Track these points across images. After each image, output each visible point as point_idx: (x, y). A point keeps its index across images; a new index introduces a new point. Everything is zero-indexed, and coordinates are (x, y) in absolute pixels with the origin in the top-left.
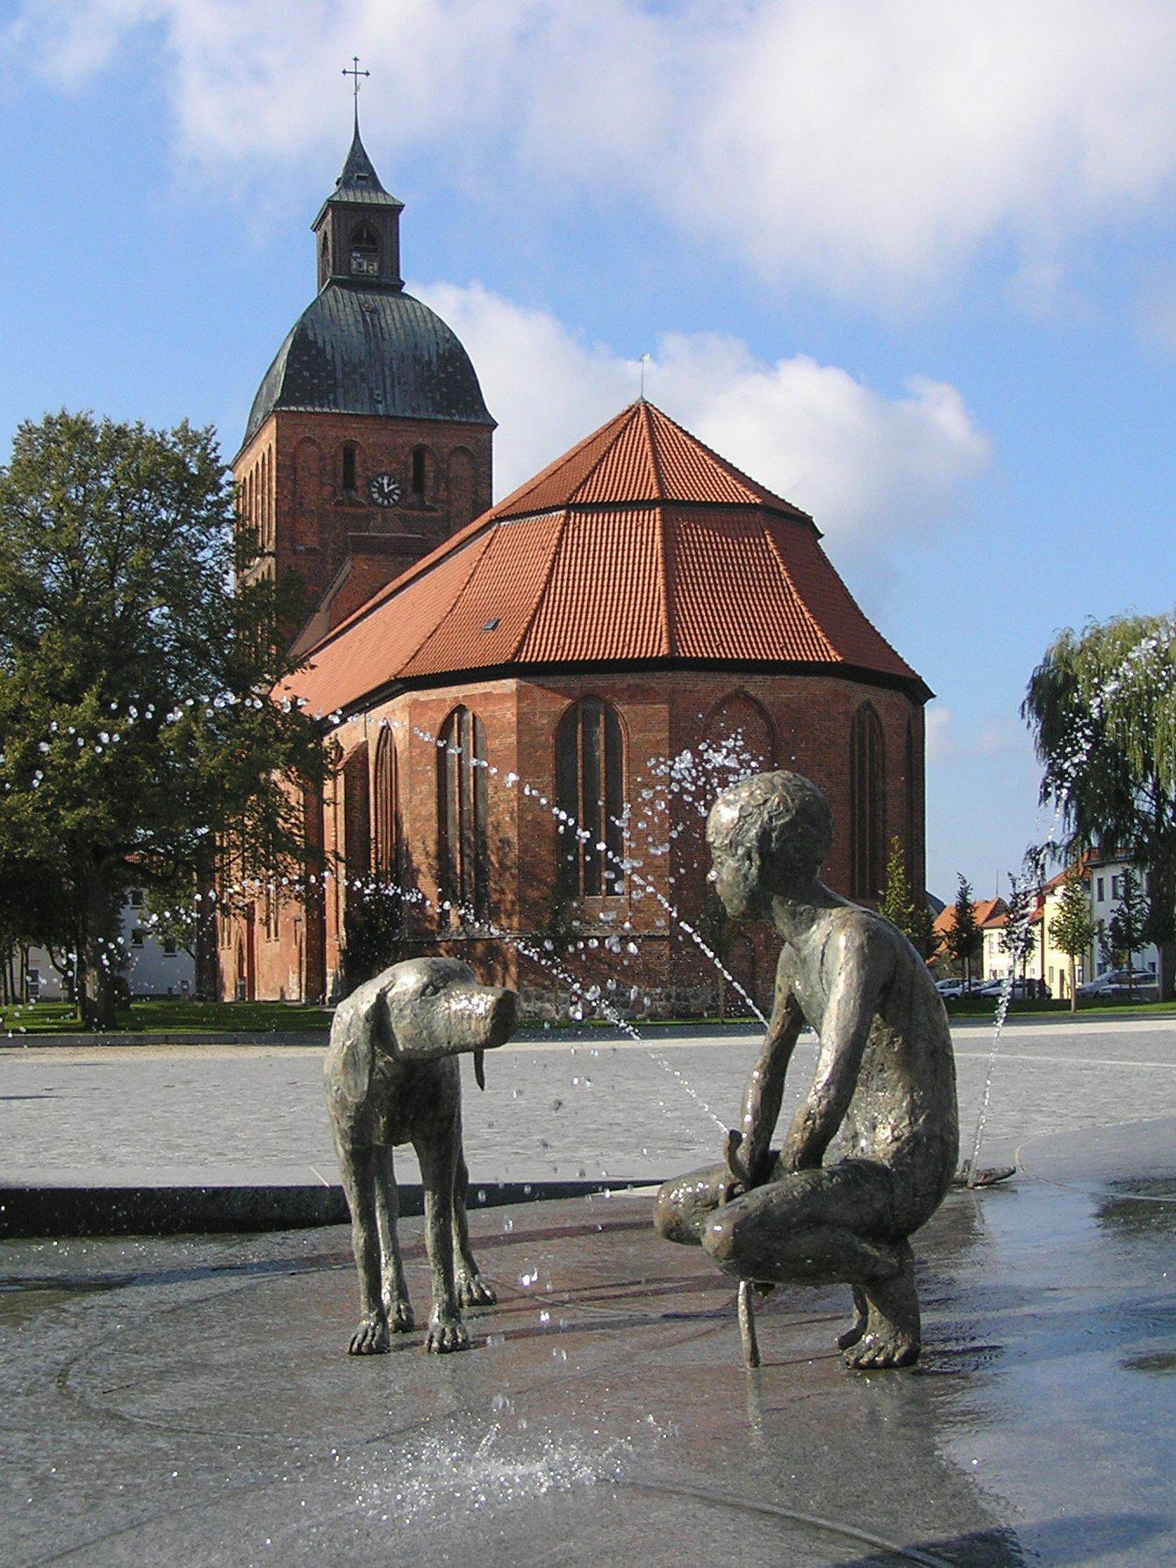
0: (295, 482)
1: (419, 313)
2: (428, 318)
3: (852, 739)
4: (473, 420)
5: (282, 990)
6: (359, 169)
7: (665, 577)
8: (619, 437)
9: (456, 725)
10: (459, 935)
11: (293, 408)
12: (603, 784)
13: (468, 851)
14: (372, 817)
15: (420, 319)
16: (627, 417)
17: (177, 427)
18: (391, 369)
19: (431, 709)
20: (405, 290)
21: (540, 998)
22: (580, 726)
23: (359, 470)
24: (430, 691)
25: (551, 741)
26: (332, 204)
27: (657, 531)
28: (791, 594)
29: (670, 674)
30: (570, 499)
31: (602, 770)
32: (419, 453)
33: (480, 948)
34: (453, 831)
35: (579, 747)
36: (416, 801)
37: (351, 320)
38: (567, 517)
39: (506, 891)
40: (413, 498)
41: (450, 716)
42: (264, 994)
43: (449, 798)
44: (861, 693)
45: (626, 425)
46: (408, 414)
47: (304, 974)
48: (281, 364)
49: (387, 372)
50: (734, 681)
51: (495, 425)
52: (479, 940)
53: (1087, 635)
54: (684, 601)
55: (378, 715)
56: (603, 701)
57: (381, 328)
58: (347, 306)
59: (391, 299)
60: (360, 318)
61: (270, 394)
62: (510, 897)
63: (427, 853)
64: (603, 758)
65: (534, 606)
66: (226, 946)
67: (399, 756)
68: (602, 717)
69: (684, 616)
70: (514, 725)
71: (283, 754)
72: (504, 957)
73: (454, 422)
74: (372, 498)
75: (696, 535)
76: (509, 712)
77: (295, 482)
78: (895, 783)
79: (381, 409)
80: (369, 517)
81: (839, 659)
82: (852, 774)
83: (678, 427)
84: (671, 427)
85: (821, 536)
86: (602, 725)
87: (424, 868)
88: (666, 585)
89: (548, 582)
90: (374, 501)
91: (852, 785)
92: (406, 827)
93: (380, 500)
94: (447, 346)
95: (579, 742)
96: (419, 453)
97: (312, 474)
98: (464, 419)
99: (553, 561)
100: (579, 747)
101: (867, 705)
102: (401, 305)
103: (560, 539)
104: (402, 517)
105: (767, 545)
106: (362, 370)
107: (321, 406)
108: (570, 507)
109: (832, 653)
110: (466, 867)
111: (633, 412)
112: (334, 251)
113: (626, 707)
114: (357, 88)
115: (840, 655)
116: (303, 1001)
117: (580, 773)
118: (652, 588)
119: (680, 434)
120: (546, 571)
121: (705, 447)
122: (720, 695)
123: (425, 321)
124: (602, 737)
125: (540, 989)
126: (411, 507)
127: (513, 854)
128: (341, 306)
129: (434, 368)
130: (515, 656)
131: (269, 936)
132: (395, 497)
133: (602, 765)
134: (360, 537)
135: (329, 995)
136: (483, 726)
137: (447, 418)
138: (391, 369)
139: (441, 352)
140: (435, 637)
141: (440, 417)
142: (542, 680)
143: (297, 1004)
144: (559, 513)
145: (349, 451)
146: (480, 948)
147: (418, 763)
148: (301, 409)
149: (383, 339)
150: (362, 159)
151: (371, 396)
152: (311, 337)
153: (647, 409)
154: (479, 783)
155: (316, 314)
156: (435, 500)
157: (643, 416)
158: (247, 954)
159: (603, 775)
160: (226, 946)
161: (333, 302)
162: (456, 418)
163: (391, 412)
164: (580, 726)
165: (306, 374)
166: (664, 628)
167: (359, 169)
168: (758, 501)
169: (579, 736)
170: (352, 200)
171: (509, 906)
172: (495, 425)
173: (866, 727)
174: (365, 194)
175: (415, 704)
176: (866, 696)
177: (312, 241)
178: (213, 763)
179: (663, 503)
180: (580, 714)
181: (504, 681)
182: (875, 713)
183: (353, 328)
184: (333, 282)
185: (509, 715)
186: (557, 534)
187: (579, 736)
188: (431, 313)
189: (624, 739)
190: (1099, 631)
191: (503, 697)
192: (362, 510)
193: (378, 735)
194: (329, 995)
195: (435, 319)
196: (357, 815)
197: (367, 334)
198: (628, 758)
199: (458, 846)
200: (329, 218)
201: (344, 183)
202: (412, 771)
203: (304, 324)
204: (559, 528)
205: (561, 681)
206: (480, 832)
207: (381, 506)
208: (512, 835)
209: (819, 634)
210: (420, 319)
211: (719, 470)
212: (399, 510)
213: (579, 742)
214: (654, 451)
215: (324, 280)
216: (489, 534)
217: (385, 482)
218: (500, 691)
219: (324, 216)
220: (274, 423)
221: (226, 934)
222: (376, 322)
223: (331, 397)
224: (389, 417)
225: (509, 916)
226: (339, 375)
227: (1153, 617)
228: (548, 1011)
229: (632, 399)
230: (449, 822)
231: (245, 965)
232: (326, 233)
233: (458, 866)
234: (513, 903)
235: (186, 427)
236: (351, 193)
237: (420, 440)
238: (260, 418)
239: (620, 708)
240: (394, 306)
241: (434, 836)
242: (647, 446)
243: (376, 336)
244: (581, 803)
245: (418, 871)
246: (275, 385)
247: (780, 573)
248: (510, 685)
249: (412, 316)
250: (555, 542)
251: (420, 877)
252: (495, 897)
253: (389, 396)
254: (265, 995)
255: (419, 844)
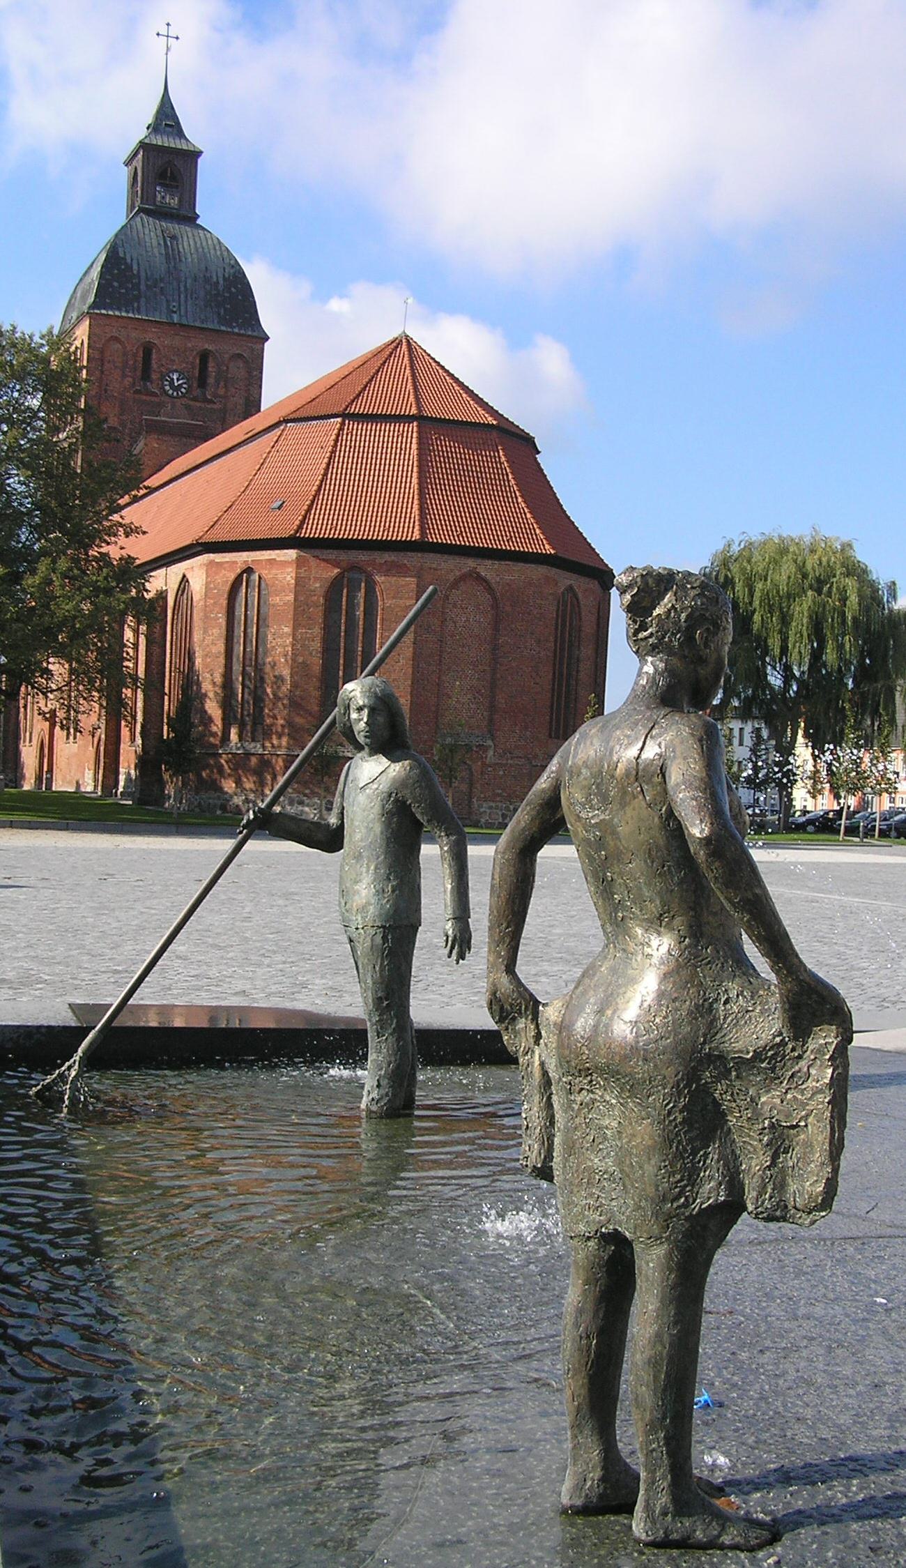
0: (102, 372)
1: (210, 242)
2: (217, 248)
3: (557, 615)
4: (250, 333)
5: (77, 783)
6: (166, 118)
7: (419, 478)
8: (385, 362)
9: (244, 583)
10: (238, 749)
11: (103, 312)
12: (361, 638)
13: (248, 683)
14: (168, 651)
15: (211, 247)
16: (392, 346)
17: (44, 332)
18: (185, 286)
19: (225, 569)
20: (199, 222)
21: (301, 803)
22: (345, 591)
23: (154, 365)
24: (224, 554)
25: (321, 600)
26: (143, 145)
27: (414, 441)
28: (516, 498)
29: (419, 555)
30: (346, 409)
31: (361, 627)
32: (204, 357)
33: (254, 760)
34: (237, 668)
35: (344, 607)
36: (209, 640)
37: (155, 243)
38: (343, 424)
39: (278, 717)
40: (197, 392)
41: (240, 576)
42: (61, 784)
43: (235, 640)
44: (566, 580)
45: (391, 353)
46: (198, 324)
47: (101, 772)
48: (95, 273)
49: (182, 289)
50: (471, 563)
51: (267, 338)
52: (253, 754)
53: (742, 546)
54: (436, 500)
55: (176, 571)
56: (365, 572)
57: (179, 252)
58: (151, 230)
59: (188, 229)
60: (162, 242)
61: (84, 297)
62: (281, 722)
63: (214, 683)
64: (362, 617)
65: (313, 493)
66: (27, 743)
67: (195, 604)
68: (363, 585)
69: (433, 508)
70: (293, 586)
71: (124, 602)
72: (273, 769)
73: (234, 333)
74: (164, 390)
75: (444, 445)
76: (288, 576)
77: (102, 372)
78: (586, 651)
79: (176, 318)
80: (161, 405)
81: (553, 552)
82: (556, 641)
83: (433, 359)
84: (426, 357)
85: (538, 452)
86: (363, 590)
87: (211, 695)
88: (420, 484)
89: (325, 474)
90: (166, 392)
91: (555, 650)
92: (198, 661)
93: (171, 392)
94: (232, 271)
95: (344, 603)
96: (204, 357)
97: (116, 367)
98: (242, 332)
99: (330, 458)
100: (344, 607)
101: (570, 589)
102: (196, 234)
103: (336, 441)
104: (188, 407)
105: (499, 458)
106: (162, 285)
107: (127, 312)
108: (345, 416)
109: (547, 547)
110: (246, 696)
111: (396, 344)
112: (143, 184)
113: (383, 578)
114: (168, 49)
115: (553, 549)
116: (99, 794)
117: (343, 628)
118: (408, 485)
119: (433, 364)
120: (324, 466)
121: (453, 375)
122: (458, 573)
123: (215, 249)
124: (362, 601)
125: (301, 796)
126: (195, 399)
127: (286, 688)
128: (147, 232)
129: (221, 288)
130: (297, 532)
131: (68, 738)
132: (183, 390)
133: (361, 623)
134: (152, 420)
135: (121, 789)
136: (267, 585)
137: (229, 330)
138: (185, 286)
139: (227, 276)
140: (230, 511)
141: (223, 328)
142: (317, 552)
143: (93, 795)
144: (336, 420)
145: (148, 350)
146: (254, 760)
147: (211, 612)
148: (111, 313)
149: (180, 261)
150: (169, 110)
151: (168, 306)
152: (121, 255)
153: (408, 341)
154: (261, 630)
155: (126, 234)
156: (215, 395)
157: (404, 343)
158: (47, 752)
159: (361, 631)
160: (27, 743)
161: (140, 227)
162: (236, 330)
163: (185, 322)
164: (345, 591)
165: (116, 284)
166: (417, 518)
167: (166, 118)
168: (495, 422)
169: (344, 599)
170: (160, 143)
171: (280, 730)
172: (267, 338)
173: (568, 606)
174: (171, 140)
175: (211, 563)
176: (569, 582)
177: (124, 174)
178: (67, 607)
179: (420, 418)
180: (345, 582)
181: (286, 551)
182: (575, 595)
183: (156, 251)
184: (141, 210)
185: (289, 578)
186: (334, 437)
187: (344, 599)
188: (219, 242)
189: (380, 603)
190: (751, 544)
191: (284, 564)
192: (153, 399)
193: (177, 586)
194: (121, 789)
195: (215, 242)
196: (156, 650)
197: (167, 254)
198: (383, 619)
199: (240, 679)
200: (140, 156)
201: (155, 128)
202: (206, 617)
203: (116, 244)
204: (336, 431)
205: (332, 554)
206: (259, 668)
207: (171, 396)
208: (286, 673)
209: (538, 531)
210: (211, 247)
211: (464, 395)
212: (184, 401)
213: (344, 603)
214: (414, 375)
215: (133, 207)
216: (277, 432)
217: (175, 377)
218: (283, 559)
219: (135, 154)
220: (88, 323)
221: (28, 734)
222: (175, 247)
223: (136, 305)
224: (182, 325)
225: (280, 736)
226: (143, 287)
227: (794, 536)
228: (307, 813)
229: (395, 333)
230: (234, 659)
231: (46, 760)
232: (136, 168)
233: (240, 695)
234: (283, 726)
235: (51, 333)
236: (159, 137)
237: (206, 346)
238: (74, 318)
239: (377, 578)
240: (190, 235)
241: (221, 670)
242: (408, 371)
243: (175, 259)
244: (342, 651)
245: (205, 695)
246: (88, 291)
247: (509, 481)
248: (291, 554)
249: (204, 244)
250: (332, 443)
251: (208, 701)
252: (268, 721)
253: (182, 308)
254: (61, 786)
255: (208, 675)
